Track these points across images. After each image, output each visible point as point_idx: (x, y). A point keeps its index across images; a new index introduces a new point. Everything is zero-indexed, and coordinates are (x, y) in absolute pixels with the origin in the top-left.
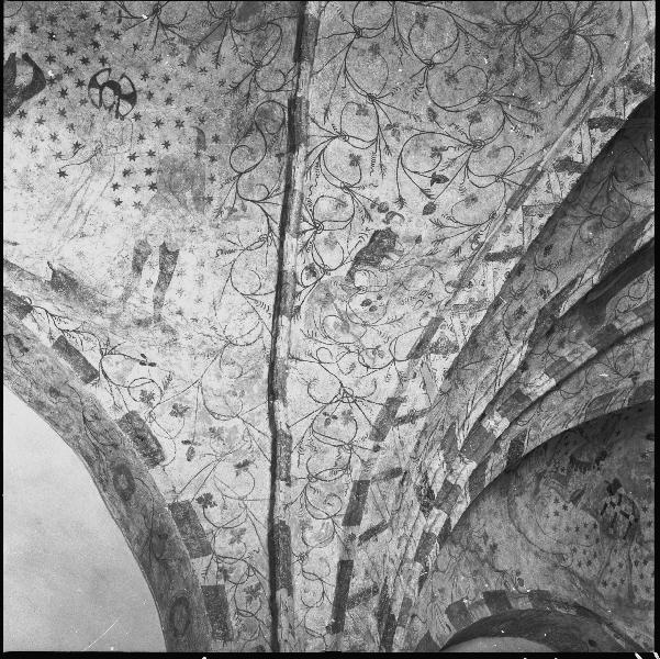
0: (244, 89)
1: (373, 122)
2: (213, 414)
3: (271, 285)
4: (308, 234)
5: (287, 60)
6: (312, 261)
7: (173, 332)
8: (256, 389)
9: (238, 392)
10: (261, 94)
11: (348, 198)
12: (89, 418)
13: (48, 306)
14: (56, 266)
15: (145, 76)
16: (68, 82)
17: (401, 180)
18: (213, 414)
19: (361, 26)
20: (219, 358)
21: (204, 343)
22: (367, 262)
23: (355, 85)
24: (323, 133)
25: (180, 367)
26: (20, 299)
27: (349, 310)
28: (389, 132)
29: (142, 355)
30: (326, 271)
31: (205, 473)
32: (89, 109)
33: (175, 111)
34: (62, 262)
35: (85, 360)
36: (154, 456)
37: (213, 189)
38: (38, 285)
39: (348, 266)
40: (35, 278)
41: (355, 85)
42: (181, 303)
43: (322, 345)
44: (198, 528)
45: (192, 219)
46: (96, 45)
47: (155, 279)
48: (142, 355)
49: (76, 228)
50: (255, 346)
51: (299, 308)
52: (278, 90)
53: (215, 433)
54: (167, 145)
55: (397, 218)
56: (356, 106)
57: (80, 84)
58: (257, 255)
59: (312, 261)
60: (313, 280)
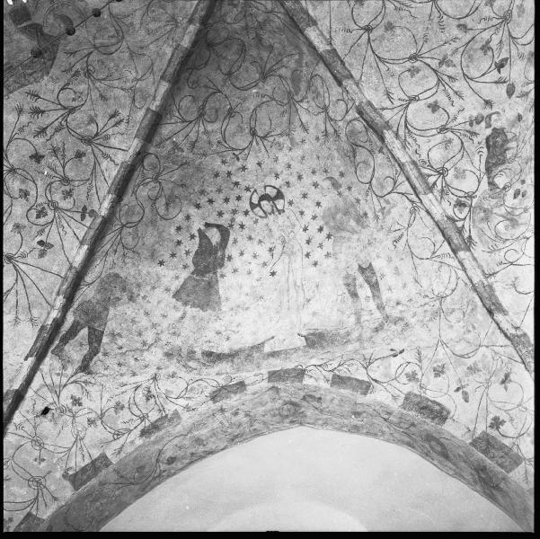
0: (331, 130)
1: (428, 71)
2: (462, 356)
3: (440, 237)
4: (439, 183)
5: (336, 90)
6: (455, 198)
7: (401, 319)
8: (479, 317)
9: (470, 328)
10: (340, 124)
11: (449, 135)
12: (386, 417)
13: (314, 361)
14: (304, 333)
15: (277, 176)
16: (240, 218)
17: (477, 89)
18: (462, 356)
19: (367, 24)
20: (442, 315)
21: (426, 311)
22: (496, 165)
23: (394, 61)
24: (396, 111)
25: (421, 340)
26: (294, 369)
27: (508, 209)
28: (444, 67)
29: (392, 350)
30: (471, 196)
31: (484, 404)
32: (262, 222)
33: (308, 180)
34: (307, 327)
35: (356, 380)
36: (440, 415)
37: (364, 207)
38: (300, 353)
39: (485, 180)
40: (296, 350)
41: (394, 61)
42: (395, 296)
43: (506, 249)
44: (502, 447)
45: (365, 235)
46: (237, 184)
47: (370, 294)
48: (392, 350)
49: (301, 299)
50: (459, 288)
51: (470, 237)
52: (347, 112)
53: (473, 370)
54: (318, 204)
55: (494, 117)
56: (407, 73)
57: (246, 213)
58: (417, 225)
59: (455, 198)
60: (467, 209)
